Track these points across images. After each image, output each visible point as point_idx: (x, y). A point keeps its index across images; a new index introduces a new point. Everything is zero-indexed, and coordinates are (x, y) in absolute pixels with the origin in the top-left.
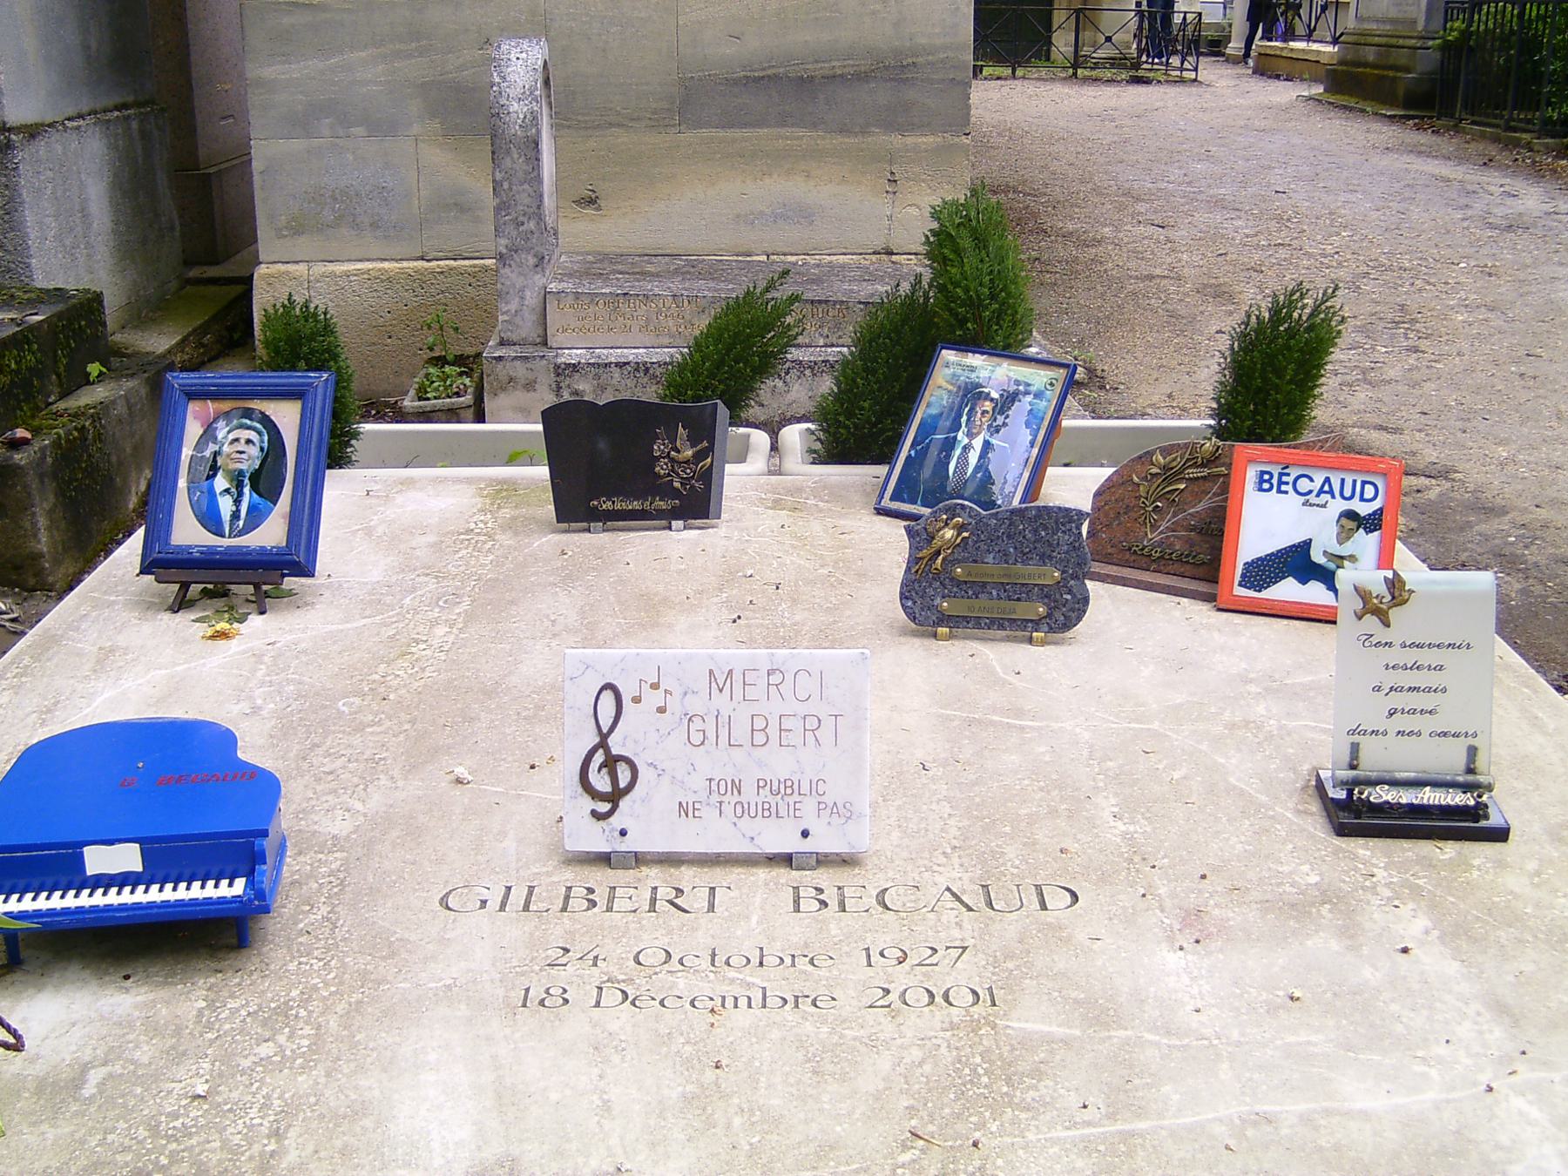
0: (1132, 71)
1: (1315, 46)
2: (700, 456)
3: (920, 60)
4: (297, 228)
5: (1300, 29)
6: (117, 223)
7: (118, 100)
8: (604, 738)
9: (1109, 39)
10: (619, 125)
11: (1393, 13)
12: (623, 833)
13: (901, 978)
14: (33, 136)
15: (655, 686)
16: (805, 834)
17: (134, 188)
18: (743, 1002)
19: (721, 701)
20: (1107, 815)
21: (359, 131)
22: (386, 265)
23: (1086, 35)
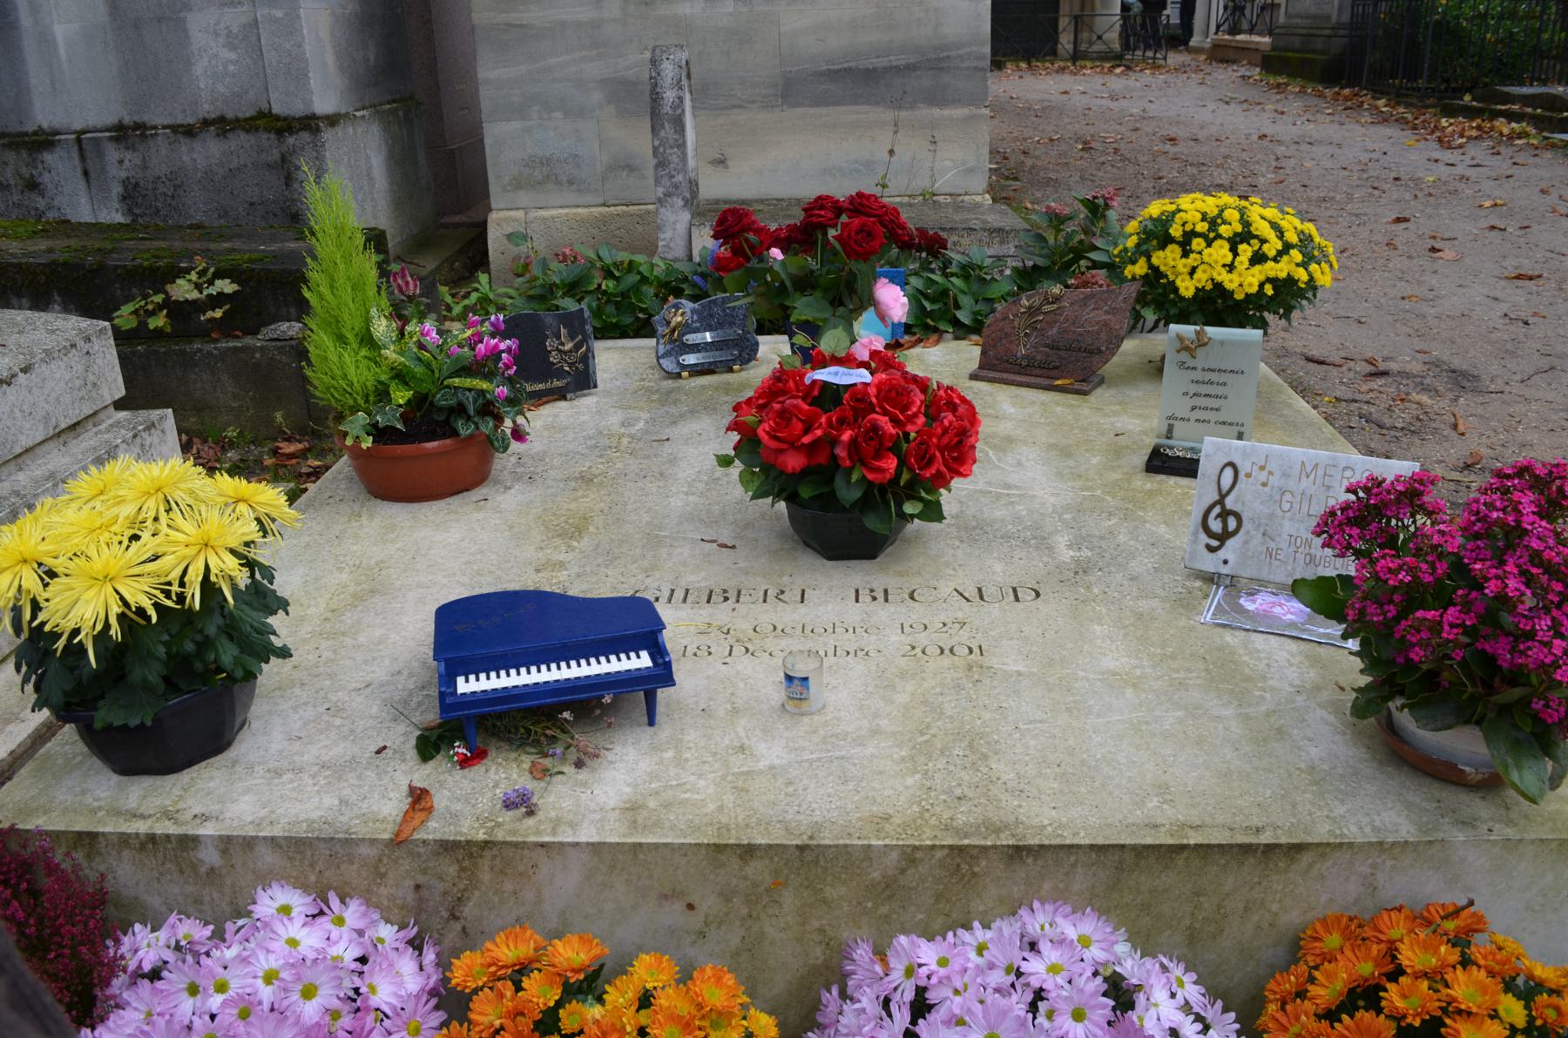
0: (1116, 59)
1: (1256, 38)
2: (577, 347)
3: (952, 54)
4: (519, 184)
5: (1245, 26)
6: (391, 184)
7: (390, 97)
9: (1100, 37)
10: (739, 107)
11: (1314, 10)
12: (1225, 562)
13: (922, 639)
15: (1262, 468)
17: (401, 160)
20: (1062, 546)
21: (558, 115)
22: (580, 210)
23: (1085, 35)
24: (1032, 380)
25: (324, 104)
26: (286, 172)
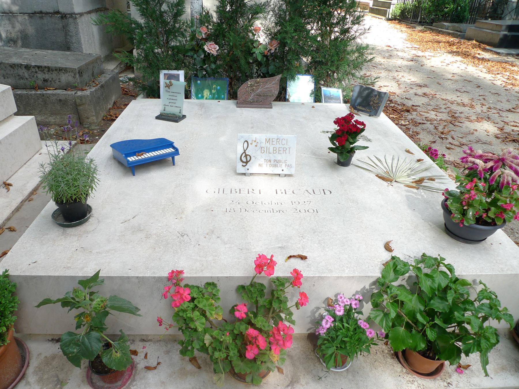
6: (100, 37)
8: (245, 151)
14: (81, 16)
15: (255, 141)
16: (283, 170)
18: (269, 211)
19: (268, 145)
24: (255, 106)
25: (78, 9)
26: (65, 28)
